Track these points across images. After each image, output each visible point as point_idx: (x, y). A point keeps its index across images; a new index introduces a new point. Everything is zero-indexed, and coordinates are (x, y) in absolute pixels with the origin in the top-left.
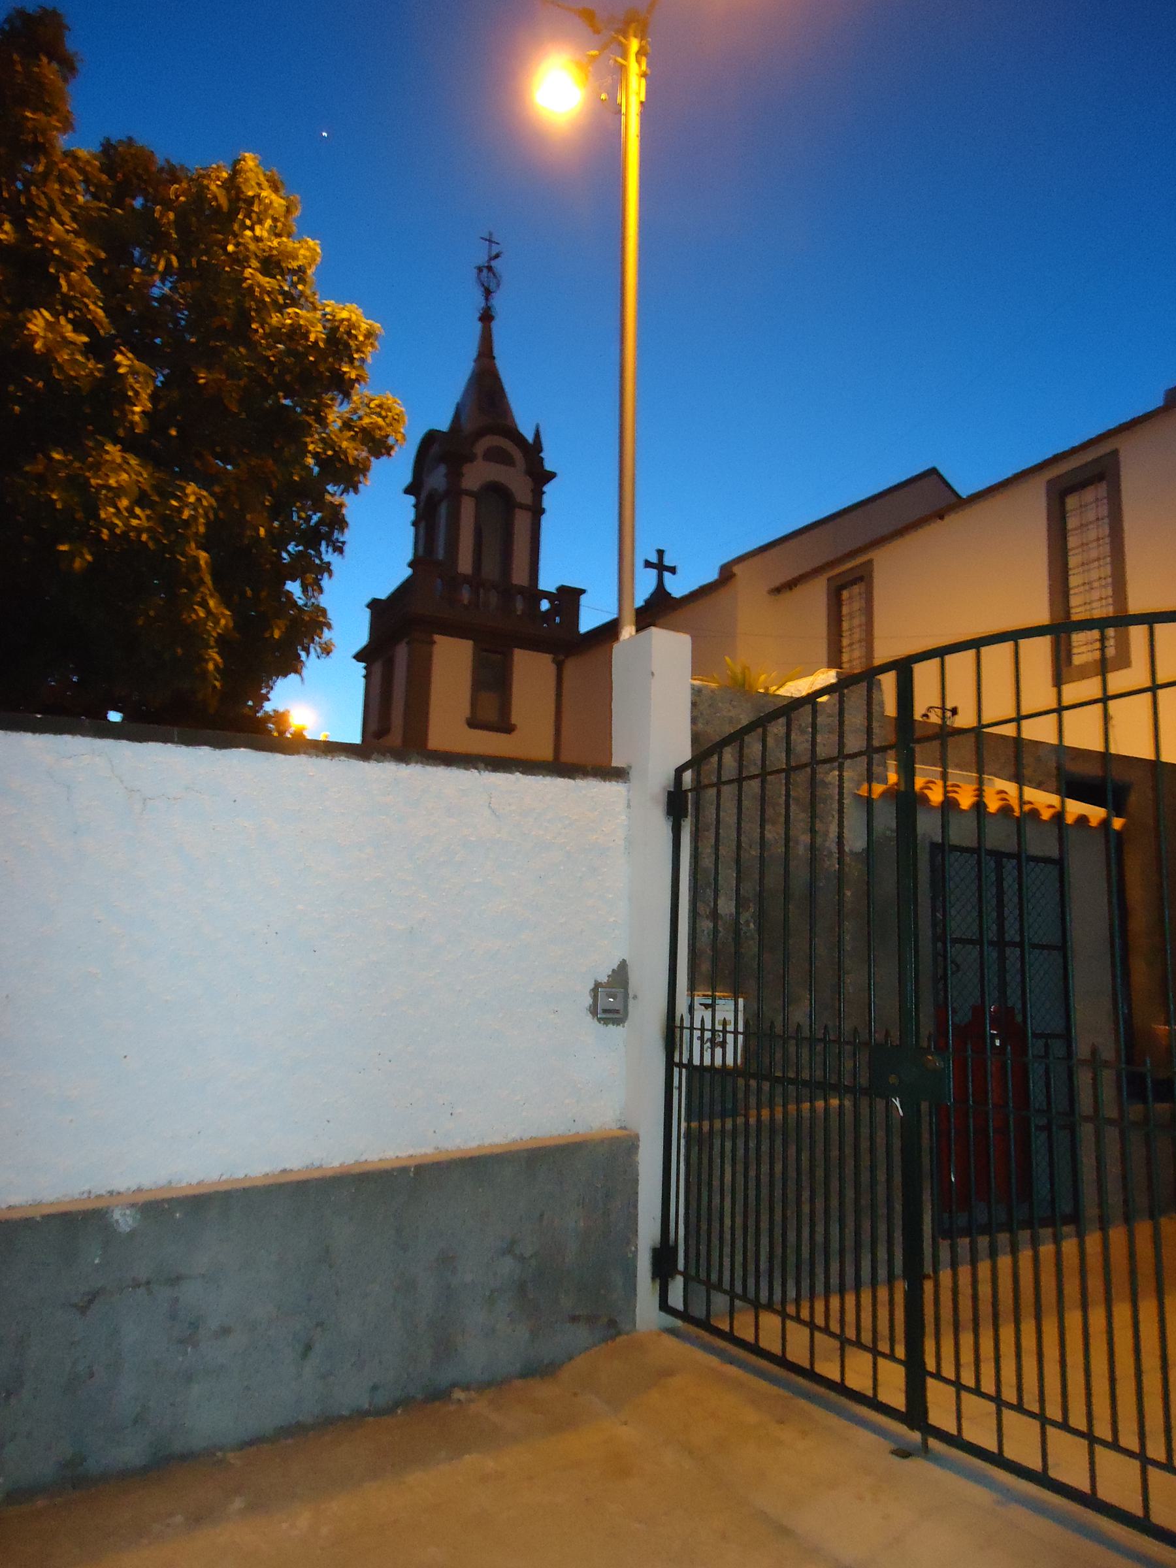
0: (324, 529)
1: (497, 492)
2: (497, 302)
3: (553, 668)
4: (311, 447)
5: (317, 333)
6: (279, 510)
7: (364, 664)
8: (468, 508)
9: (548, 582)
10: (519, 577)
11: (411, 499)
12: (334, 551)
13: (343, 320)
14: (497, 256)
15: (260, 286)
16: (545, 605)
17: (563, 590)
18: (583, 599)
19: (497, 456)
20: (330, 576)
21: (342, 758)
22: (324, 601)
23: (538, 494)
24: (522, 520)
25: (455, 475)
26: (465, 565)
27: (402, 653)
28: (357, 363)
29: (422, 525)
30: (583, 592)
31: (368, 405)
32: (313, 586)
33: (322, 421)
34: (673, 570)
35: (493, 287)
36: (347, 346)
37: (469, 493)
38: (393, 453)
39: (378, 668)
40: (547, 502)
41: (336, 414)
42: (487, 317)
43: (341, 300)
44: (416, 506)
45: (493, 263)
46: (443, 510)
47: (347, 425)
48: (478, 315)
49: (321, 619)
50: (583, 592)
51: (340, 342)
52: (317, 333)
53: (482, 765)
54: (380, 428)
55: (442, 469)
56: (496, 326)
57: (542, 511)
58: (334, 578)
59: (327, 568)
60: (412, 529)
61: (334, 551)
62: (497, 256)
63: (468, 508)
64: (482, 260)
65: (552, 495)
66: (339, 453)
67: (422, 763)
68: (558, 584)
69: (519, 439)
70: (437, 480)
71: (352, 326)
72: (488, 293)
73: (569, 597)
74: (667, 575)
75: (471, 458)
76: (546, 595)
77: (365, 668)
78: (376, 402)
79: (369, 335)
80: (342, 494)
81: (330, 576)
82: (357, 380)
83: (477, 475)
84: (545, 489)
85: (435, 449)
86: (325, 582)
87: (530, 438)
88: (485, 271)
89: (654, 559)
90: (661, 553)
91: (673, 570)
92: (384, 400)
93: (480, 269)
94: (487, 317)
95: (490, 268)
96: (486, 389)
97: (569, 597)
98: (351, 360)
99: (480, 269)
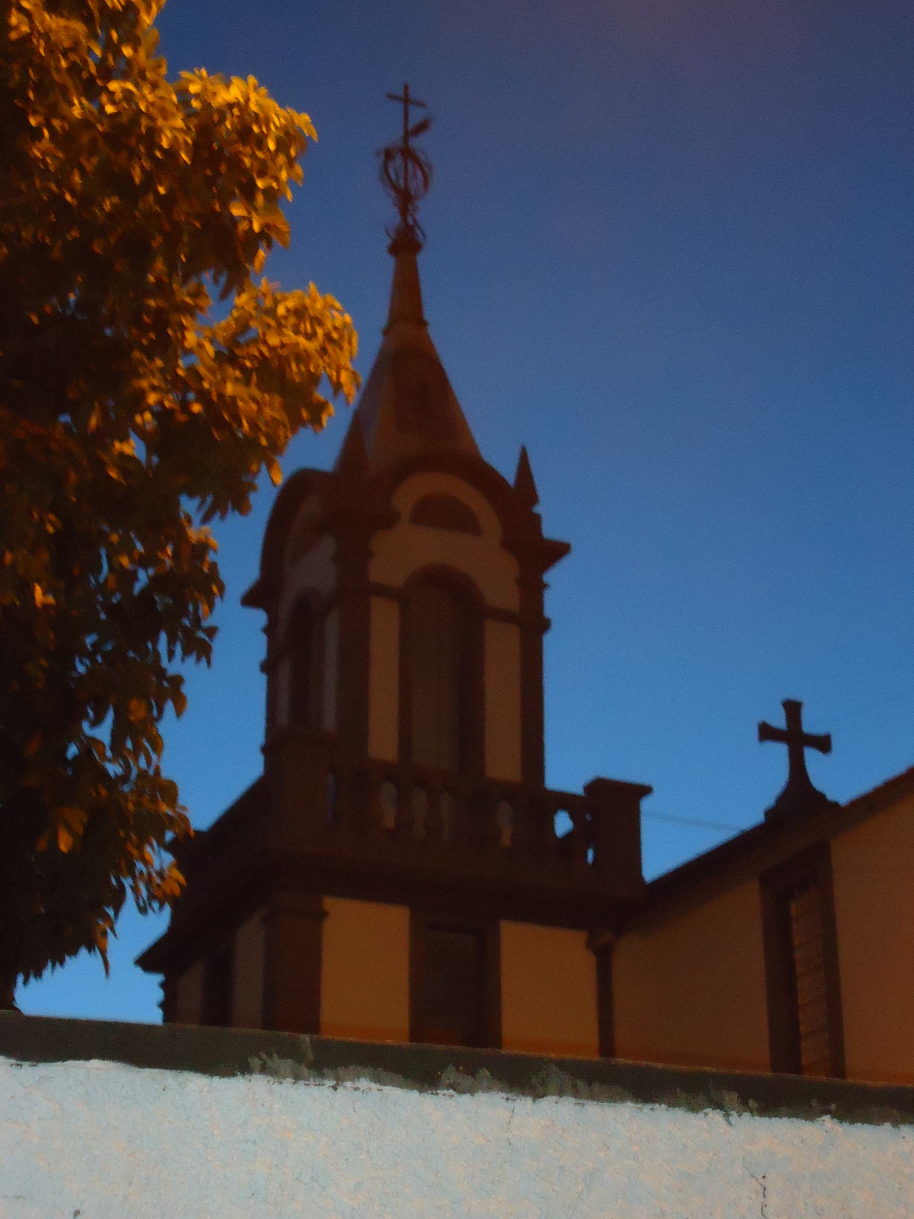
0: (161, 601)
1: (447, 587)
2: (426, 214)
3: (586, 962)
4: (152, 398)
5: (173, 131)
6: (69, 559)
7: (159, 978)
8: (384, 624)
9: (565, 773)
10: (502, 765)
11: (260, 617)
12: (186, 652)
13: (231, 106)
14: (423, 127)
15: (46, 36)
16: (563, 824)
17: (600, 789)
18: (646, 805)
19: (438, 514)
20: (180, 709)
21: (364, 1083)
22: (171, 766)
23: (533, 589)
24: (500, 646)
25: (354, 559)
26: (383, 743)
27: (250, 942)
28: (260, 199)
29: (285, 671)
30: (645, 790)
31: (272, 312)
32: (137, 733)
33: (167, 346)
34: (823, 744)
35: (415, 185)
36: (235, 163)
37: (383, 591)
38: (325, 419)
39: (193, 982)
40: (553, 605)
41: (199, 338)
42: (406, 245)
43: (226, 70)
44: (269, 630)
45: (416, 143)
46: (332, 628)
47: (228, 357)
48: (389, 241)
49: (165, 809)
50: (645, 790)
51: (222, 154)
52: (173, 131)
53: (731, 1097)
54: (302, 357)
55: (327, 546)
56: (427, 263)
57: (544, 625)
58: (186, 716)
59: (174, 690)
60: (260, 682)
61: (186, 652)
62: (423, 127)
63: (384, 624)
64: (393, 135)
65: (561, 587)
66: (220, 411)
67: (576, 1094)
68: (588, 776)
69: (483, 476)
70: (317, 570)
71: (247, 131)
72: (405, 200)
73: (614, 806)
74: (811, 756)
75: (388, 521)
76: (564, 801)
77: (163, 986)
78: (291, 304)
79: (288, 137)
80: (206, 519)
81: (180, 709)
82: (265, 236)
83: (401, 553)
84: (549, 577)
85: (311, 506)
86: (168, 725)
87: (509, 472)
88: (399, 161)
89: (779, 721)
90: (793, 709)
91: (823, 744)
92: (307, 301)
93: (388, 155)
94: (406, 245)
95: (407, 153)
96: (411, 377)
97: (614, 806)
98: (249, 193)
99: (388, 155)
